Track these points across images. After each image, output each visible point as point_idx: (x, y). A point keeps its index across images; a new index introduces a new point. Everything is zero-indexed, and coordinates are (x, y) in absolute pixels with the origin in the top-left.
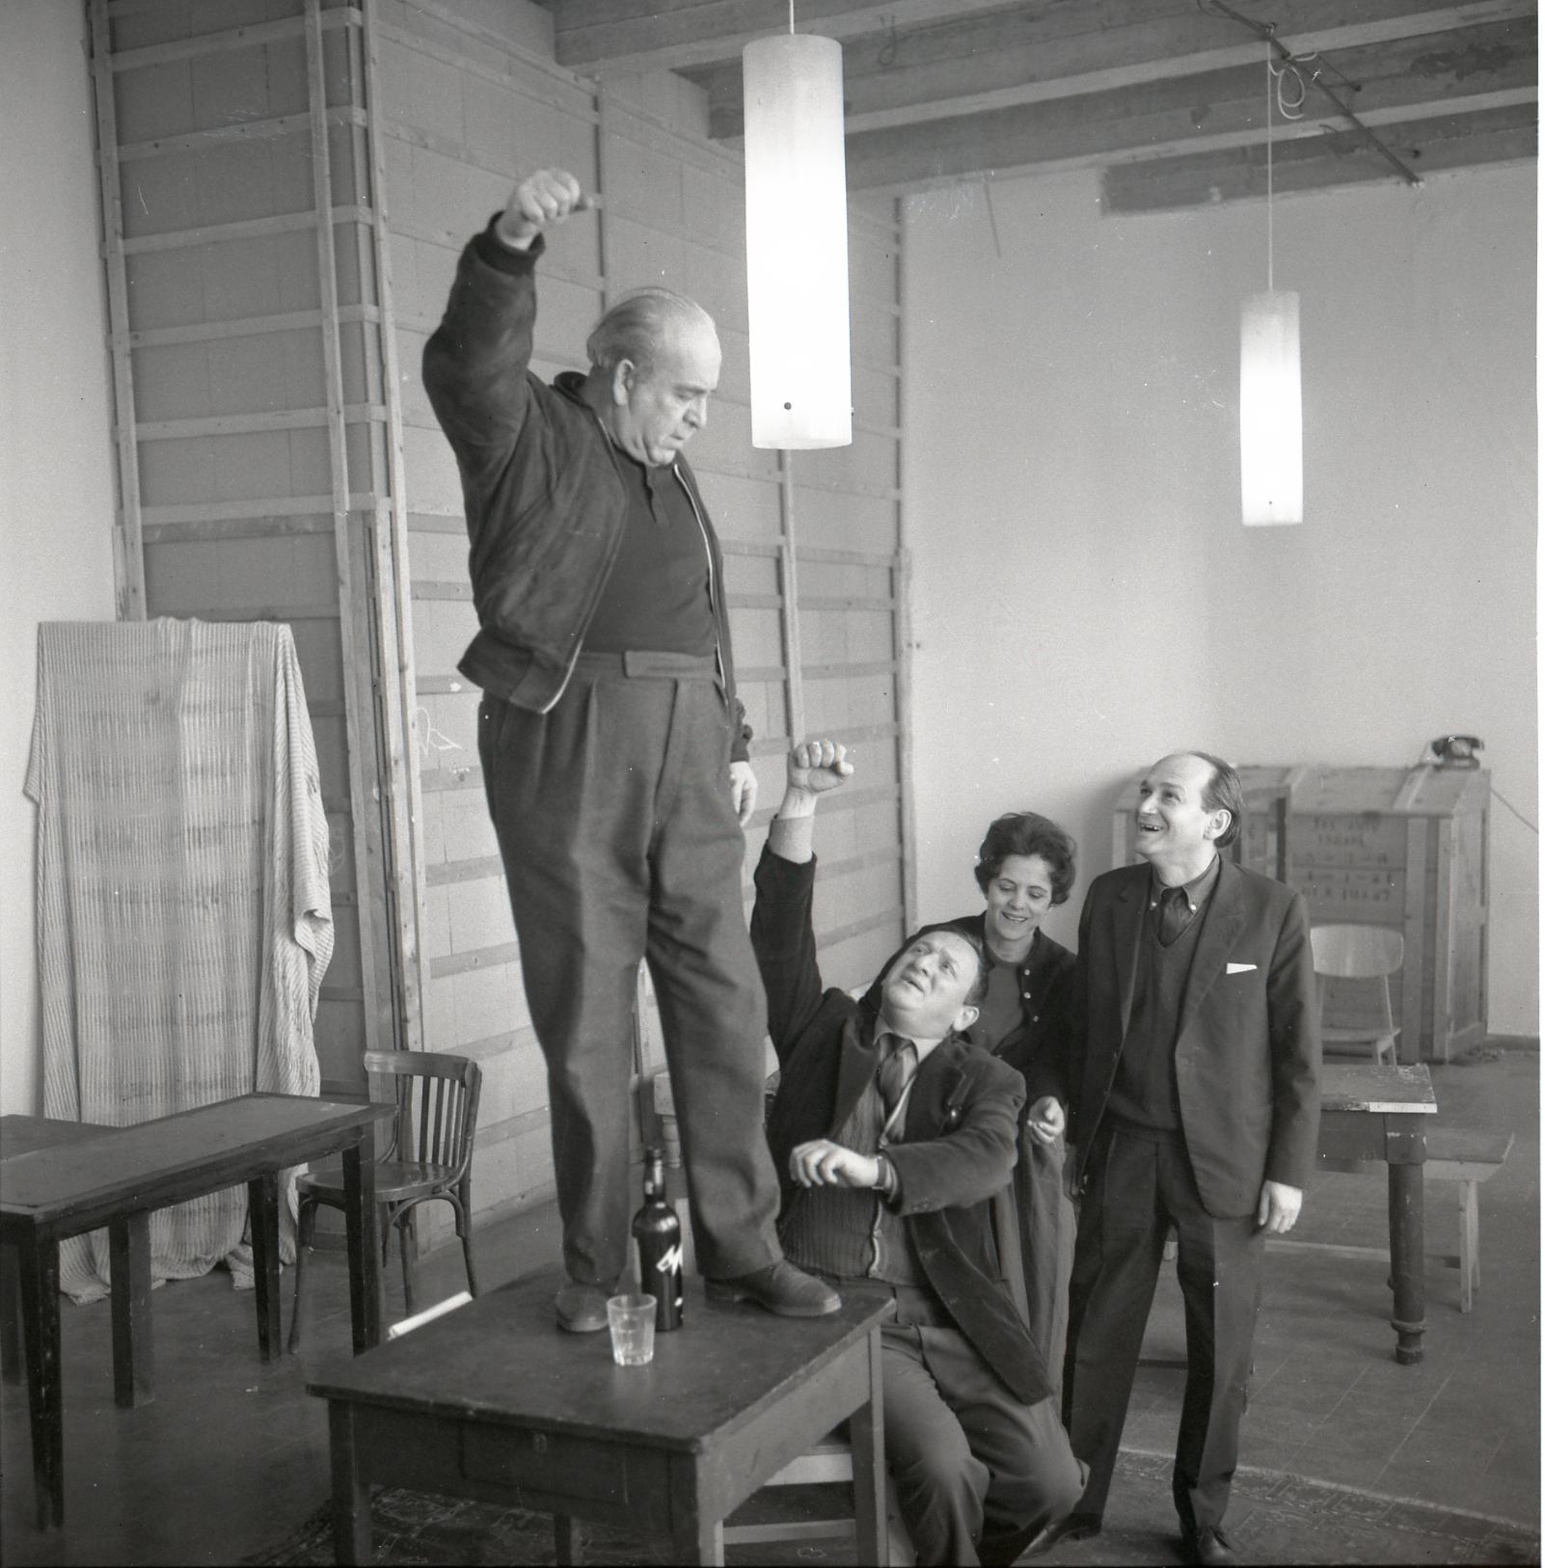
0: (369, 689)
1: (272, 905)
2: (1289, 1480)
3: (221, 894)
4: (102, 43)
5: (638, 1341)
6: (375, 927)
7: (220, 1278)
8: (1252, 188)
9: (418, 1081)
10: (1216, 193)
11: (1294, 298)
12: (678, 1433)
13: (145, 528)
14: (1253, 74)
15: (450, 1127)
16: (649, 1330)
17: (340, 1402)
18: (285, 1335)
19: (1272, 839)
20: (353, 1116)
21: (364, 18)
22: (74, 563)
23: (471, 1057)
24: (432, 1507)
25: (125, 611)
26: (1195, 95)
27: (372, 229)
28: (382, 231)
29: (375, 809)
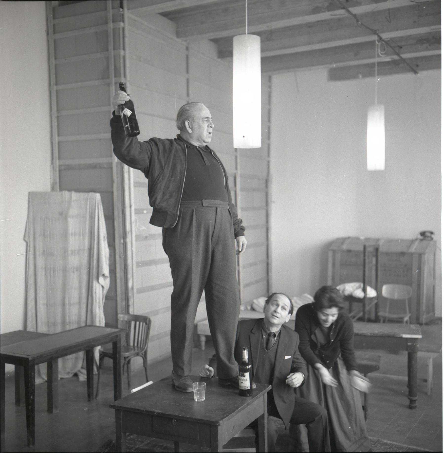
0: (121, 212)
1: (93, 272)
2: (378, 440)
3: (78, 269)
4: (51, 31)
5: (201, 395)
6: (121, 278)
7: (75, 378)
9: (133, 323)
10: (360, 76)
11: (383, 107)
12: (213, 420)
13: (59, 166)
15: (142, 336)
16: (204, 392)
17: (119, 410)
18: (95, 394)
19: (374, 260)
20: (114, 333)
21: (124, 25)
24: (137, 443)
25: (53, 189)
26: (357, 49)
29: (122, 246)
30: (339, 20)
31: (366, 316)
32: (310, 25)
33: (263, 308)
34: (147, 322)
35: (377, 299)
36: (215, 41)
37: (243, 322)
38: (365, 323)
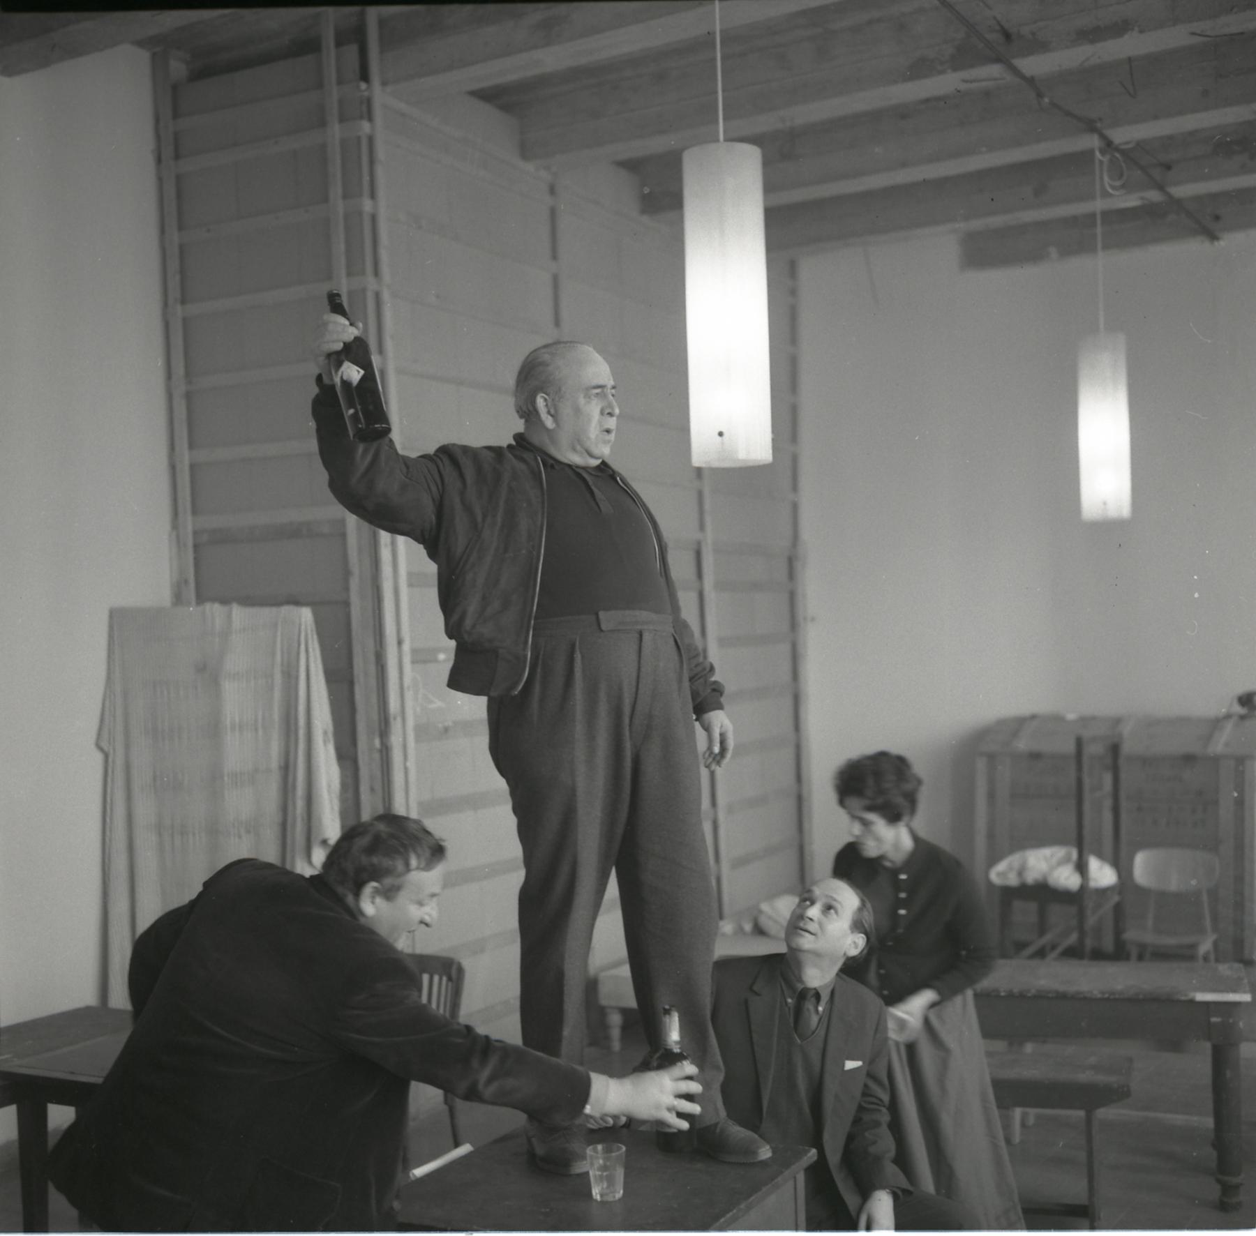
0: (372, 658)
5: (610, 1181)
8: (1083, 246)
10: (1053, 251)
13: (195, 533)
14: (1082, 160)
16: (620, 1174)
19: (1108, 779)
22: (141, 564)
23: (451, 955)
25: (178, 599)
26: (1038, 176)
27: (377, 296)
28: (386, 296)
29: (377, 756)
30: (987, 94)
31: (1089, 943)
32: (902, 113)
33: (785, 924)
34: (454, 972)
35: (1120, 893)
36: (632, 166)
37: (726, 965)
38: (1085, 962)
